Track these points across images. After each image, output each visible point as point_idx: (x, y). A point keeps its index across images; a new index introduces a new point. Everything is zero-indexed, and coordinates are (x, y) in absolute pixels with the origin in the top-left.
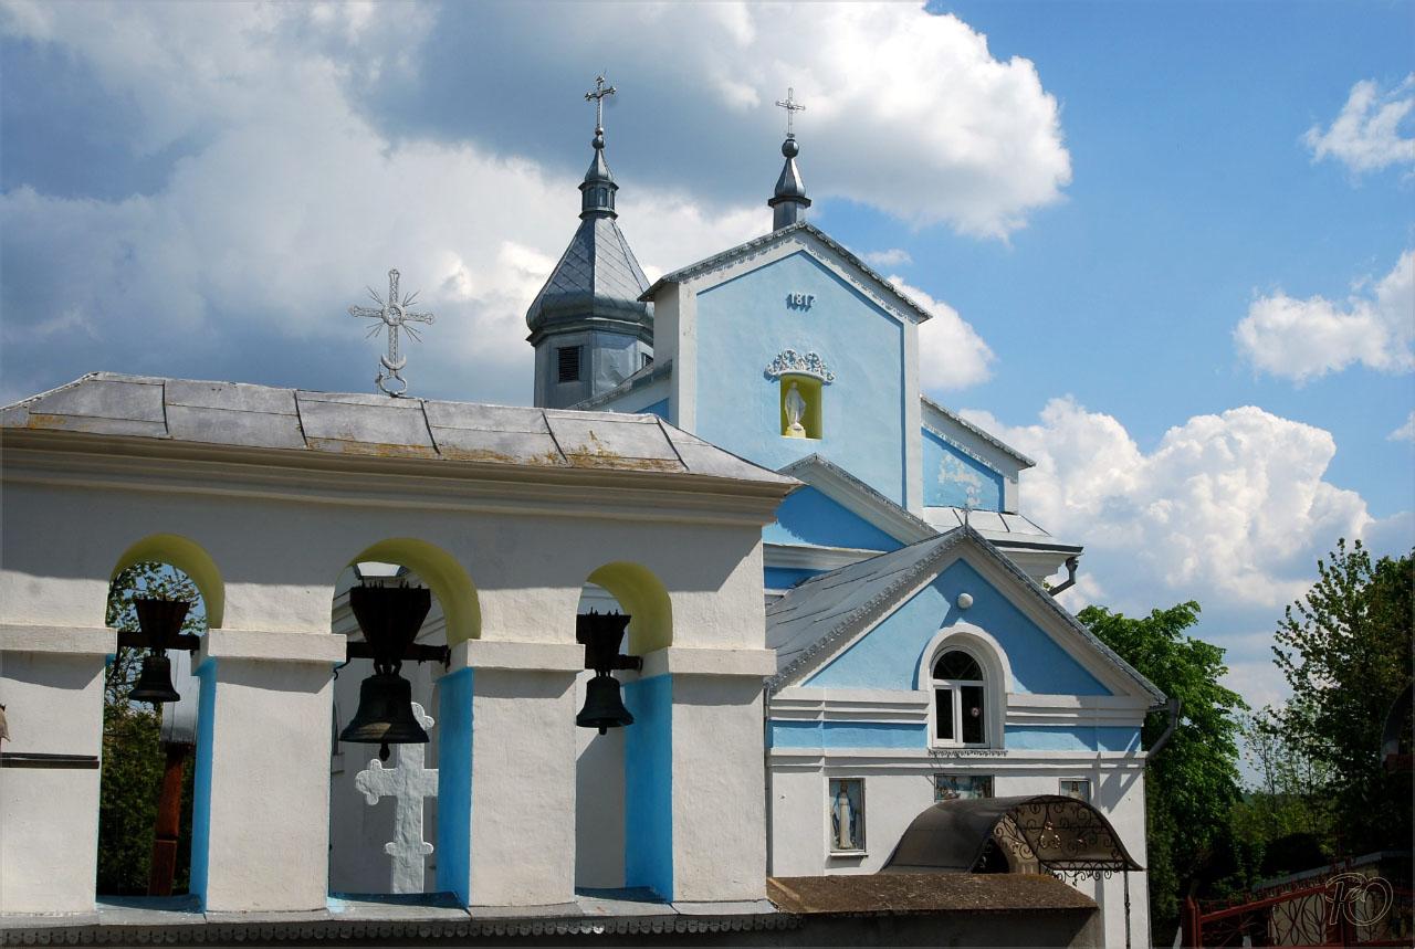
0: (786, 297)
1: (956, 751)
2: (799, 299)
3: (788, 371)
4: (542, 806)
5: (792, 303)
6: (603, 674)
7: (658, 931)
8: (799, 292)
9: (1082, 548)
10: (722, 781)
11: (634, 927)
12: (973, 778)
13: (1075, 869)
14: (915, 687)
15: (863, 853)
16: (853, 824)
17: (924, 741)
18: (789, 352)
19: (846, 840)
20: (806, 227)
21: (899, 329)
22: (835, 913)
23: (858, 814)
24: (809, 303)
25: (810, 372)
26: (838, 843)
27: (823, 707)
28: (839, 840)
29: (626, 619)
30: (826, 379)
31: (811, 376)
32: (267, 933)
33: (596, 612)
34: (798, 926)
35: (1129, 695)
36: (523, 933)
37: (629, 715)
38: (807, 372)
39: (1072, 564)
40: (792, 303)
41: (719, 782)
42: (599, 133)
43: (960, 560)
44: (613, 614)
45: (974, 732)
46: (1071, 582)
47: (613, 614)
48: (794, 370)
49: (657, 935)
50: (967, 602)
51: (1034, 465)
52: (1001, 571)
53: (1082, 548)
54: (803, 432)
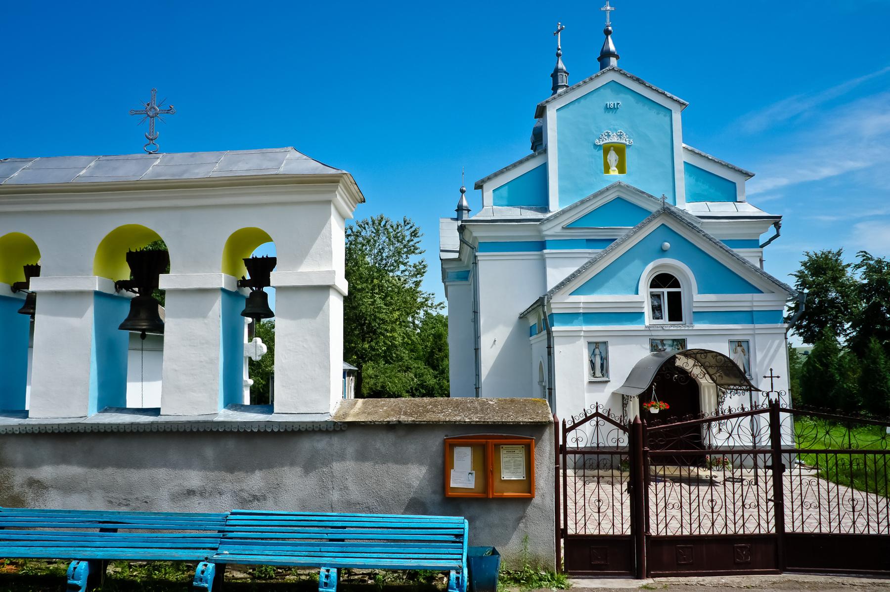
0: (605, 105)
1: (662, 326)
2: (611, 105)
3: (607, 141)
4: (201, 362)
5: (608, 109)
6: (259, 289)
7: (256, 430)
8: (611, 103)
9: (781, 217)
10: (305, 346)
11: (242, 428)
12: (674, 340)
13: (730, 389)
14: (637, 293)
15: (608, 380)
16: (602, 365)
17: (643, 322)
18: (607, 132)
19: (598, 373)
20: (613, 69)
21: (668, 115)
22: (363, 422)
23: (604, 360)
24: (617, 106)
25: (619, 141)
26: (594, 375)
27: (582, 305)
28: (594, 373)
29: (244, 260)
30: (628, 144)
31: (621, 143)
32: (50, 429)
33: (256, 257)
34: (341, 429)
35: (774, 293)
36: (281, 430)
37: (272, 313)
38: (617, 141)
39: (777, 226)
40: (608, 109)
41: (303, 346)
42: (559, 49)
43: (663, 224)
44: (265, 257)
45: (676, 314)
46: (777, 235)
47: (265, 257)
48: (610, 141)
49: (241, 432)
50: (667, 247)
51: (754, 175)
52: (687, 228)
53: (781, 217)
54: (617, 171)
